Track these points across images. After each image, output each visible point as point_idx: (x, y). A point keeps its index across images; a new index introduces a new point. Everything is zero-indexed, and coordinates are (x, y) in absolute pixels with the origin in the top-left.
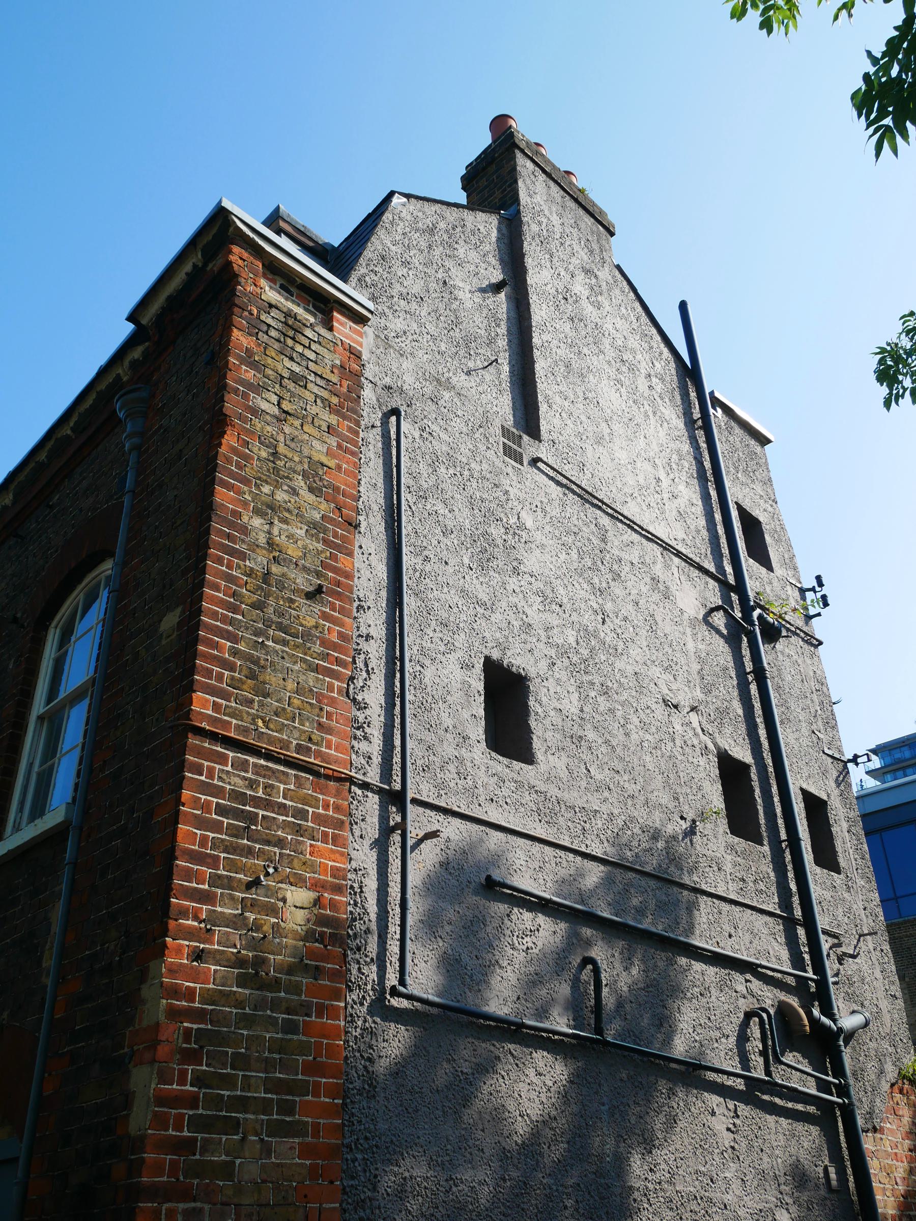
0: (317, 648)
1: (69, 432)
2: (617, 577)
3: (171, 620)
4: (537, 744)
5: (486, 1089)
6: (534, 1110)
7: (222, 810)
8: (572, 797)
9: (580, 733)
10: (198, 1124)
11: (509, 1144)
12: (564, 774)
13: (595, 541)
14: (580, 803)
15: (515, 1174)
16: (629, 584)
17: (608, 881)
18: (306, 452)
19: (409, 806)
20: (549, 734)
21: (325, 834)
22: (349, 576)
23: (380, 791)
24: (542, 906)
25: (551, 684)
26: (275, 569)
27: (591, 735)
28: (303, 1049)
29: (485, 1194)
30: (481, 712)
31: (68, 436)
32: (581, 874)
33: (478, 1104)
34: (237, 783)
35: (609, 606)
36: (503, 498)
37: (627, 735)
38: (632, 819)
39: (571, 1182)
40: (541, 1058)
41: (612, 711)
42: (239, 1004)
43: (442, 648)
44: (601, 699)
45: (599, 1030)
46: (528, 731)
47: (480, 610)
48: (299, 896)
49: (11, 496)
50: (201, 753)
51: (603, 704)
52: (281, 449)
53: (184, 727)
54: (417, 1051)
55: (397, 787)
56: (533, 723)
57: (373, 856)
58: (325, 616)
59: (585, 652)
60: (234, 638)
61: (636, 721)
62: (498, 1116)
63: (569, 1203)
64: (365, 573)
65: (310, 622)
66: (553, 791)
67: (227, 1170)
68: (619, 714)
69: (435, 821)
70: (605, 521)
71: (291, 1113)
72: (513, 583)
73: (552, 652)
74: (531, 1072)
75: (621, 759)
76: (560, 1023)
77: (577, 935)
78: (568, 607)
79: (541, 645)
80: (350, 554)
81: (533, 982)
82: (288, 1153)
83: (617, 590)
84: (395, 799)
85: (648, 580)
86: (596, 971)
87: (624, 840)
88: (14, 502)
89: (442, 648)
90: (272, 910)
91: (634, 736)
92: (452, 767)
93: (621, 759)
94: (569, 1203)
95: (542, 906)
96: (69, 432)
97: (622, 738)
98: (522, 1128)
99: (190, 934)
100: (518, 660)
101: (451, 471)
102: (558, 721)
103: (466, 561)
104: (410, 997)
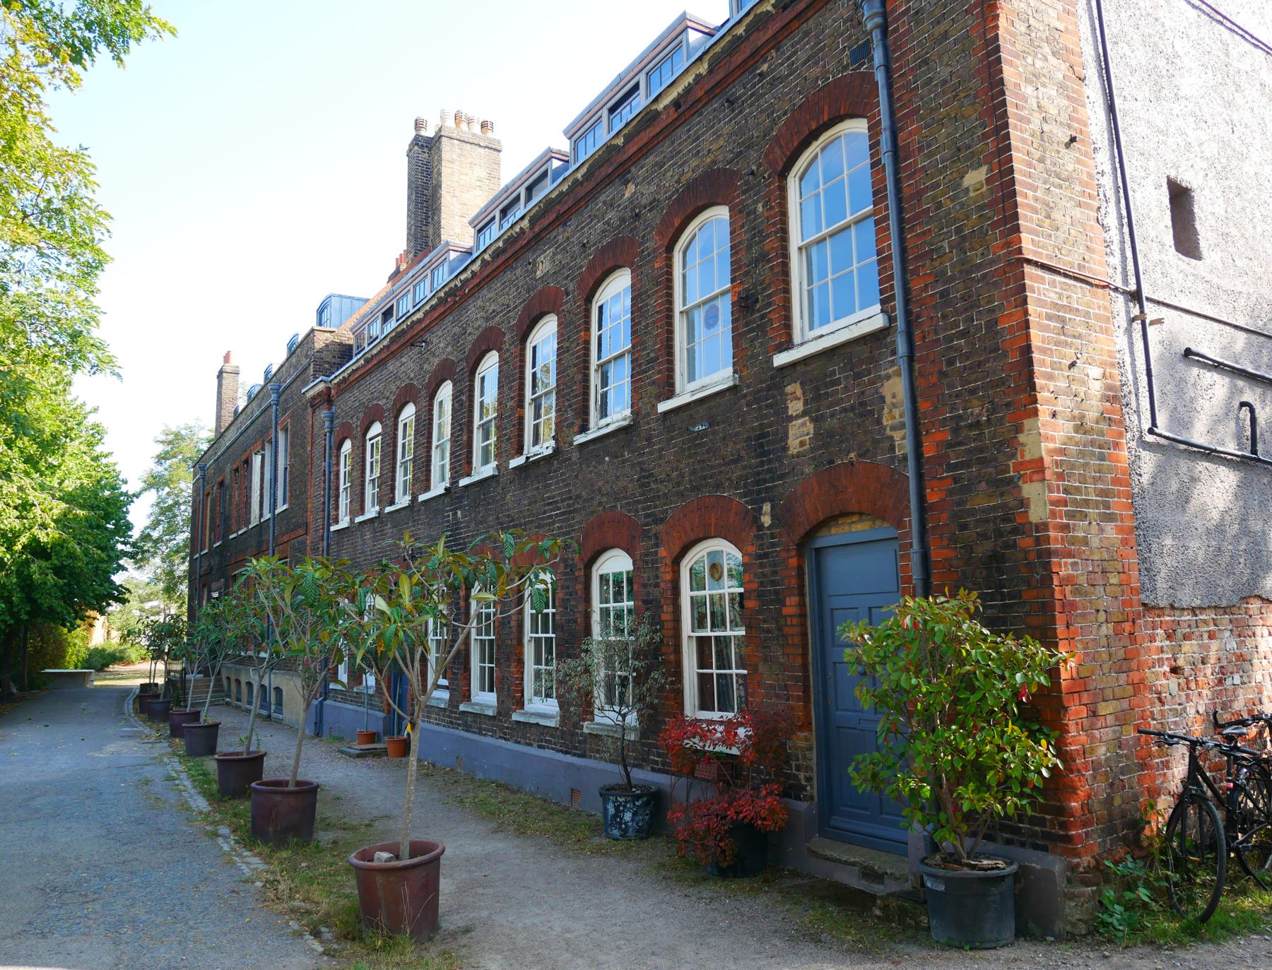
0: (1078, 188)
1: (770, 8)
2: (1238, 88)
3: (975, 177)
4: (1203, 245)
5: (1196, 492)
6: (1221, 505)
7: (1049, 317)
8: (1226, 283)
9: (1227, 230)
10: (1071, 515)
11: (1209, 525)
12: (1220, 265)
13: (1222, 57)
14: (1230, 287)
15: (1214, 543)
16: (1246, 93)
17: (1249, 344)
18: (1046, 20)
19: (1145, 303)
20: (1209, 234)
21: (1101, 328)
22: (1086, 125)
23: (1124, 293)
24: (1217, 367)
25: (1206, 192)
26: (1046, 128)
27: (1234, 231)
28: (1110, 470)
29: (1201, 554)
30: (1170, 224)
31: (768, 12)
32: (1233, 341)
33: (1193, 502)
34: (1052, 297)
35: (1235, 117)
36: (1162, 30)
37: (1254, 227)
38: (1262, 296)
39: (1242, 548)
40: (1223, 471)
41: (1243, 209)
42: (1077, 444)
43: (1143, 174)
44: (1237, 200)
45: (1254, 451)
46: (1195, 232)
47: (1161, 137)
48: (1095, 372)
49: (706, 66)
50: (1034, 279)
51: (1239, 203)
52: (1032, 21)
53: (1018, 262)
54: (1160, 470)
55: (1133, 287)
56: (1198, 226)
57: (1125, 339)
58: (1078, 161)
59: (1224, 160)
60: (1035, 189)
61: (1258, 215)
62: (1204, 510)
63: (1242, 560)
64: (1093, 121)
65: (1070, 167)
66: (1215, 281)
67: (1085, 541)
68: (1248, 210)
69: (1163, 312)
70: (1226, 34)
71: (1109, 508)
72: (1177, 108)
73: (1205, 165)
74: (1218, 481)
75: (1252, 248)
76: (1231, 447)
77: (1236, 386)
78: (1210, 122)
79: (1198, 160)
80: (1083, 106)
81: (1217, 421)
82: (1110, 531)
83: (1239, 100)
84: (1136, 296)
85: (1258, 86)
86: (1252, 411)
87: (1256, 313)
88: (710, 71)
89: (1143, 174)
90: (1083, 383)
91: (1259, 229)
92: (1158, 269)
93: (1252, 248)
94: (1242, 560)
95: (1217, 367)
96: (770, 8)
97: (1251, 230)
98: (1215, 515)
99: (1048, 402)
100: (1187, 178)
101: (1129, 13)
102: (1213, 222)
103: (1147, 95)
104: (1160, 435)
